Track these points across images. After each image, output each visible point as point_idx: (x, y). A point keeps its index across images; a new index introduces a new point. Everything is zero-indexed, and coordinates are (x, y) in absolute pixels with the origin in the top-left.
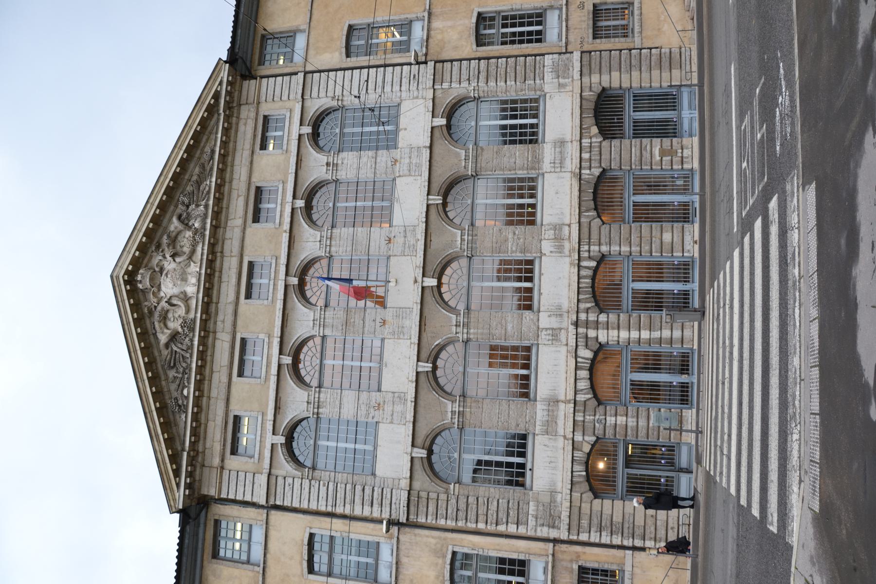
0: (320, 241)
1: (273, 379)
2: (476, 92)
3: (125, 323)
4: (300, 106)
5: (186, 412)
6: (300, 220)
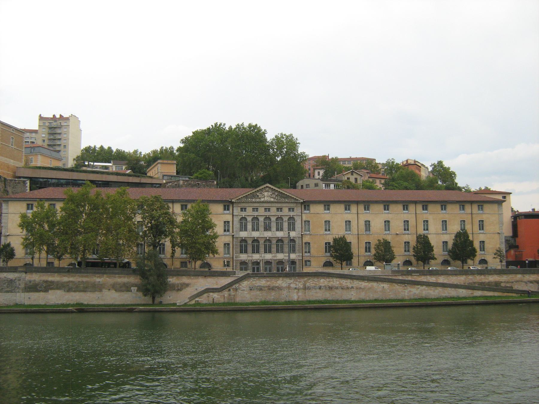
1: (252, 214)
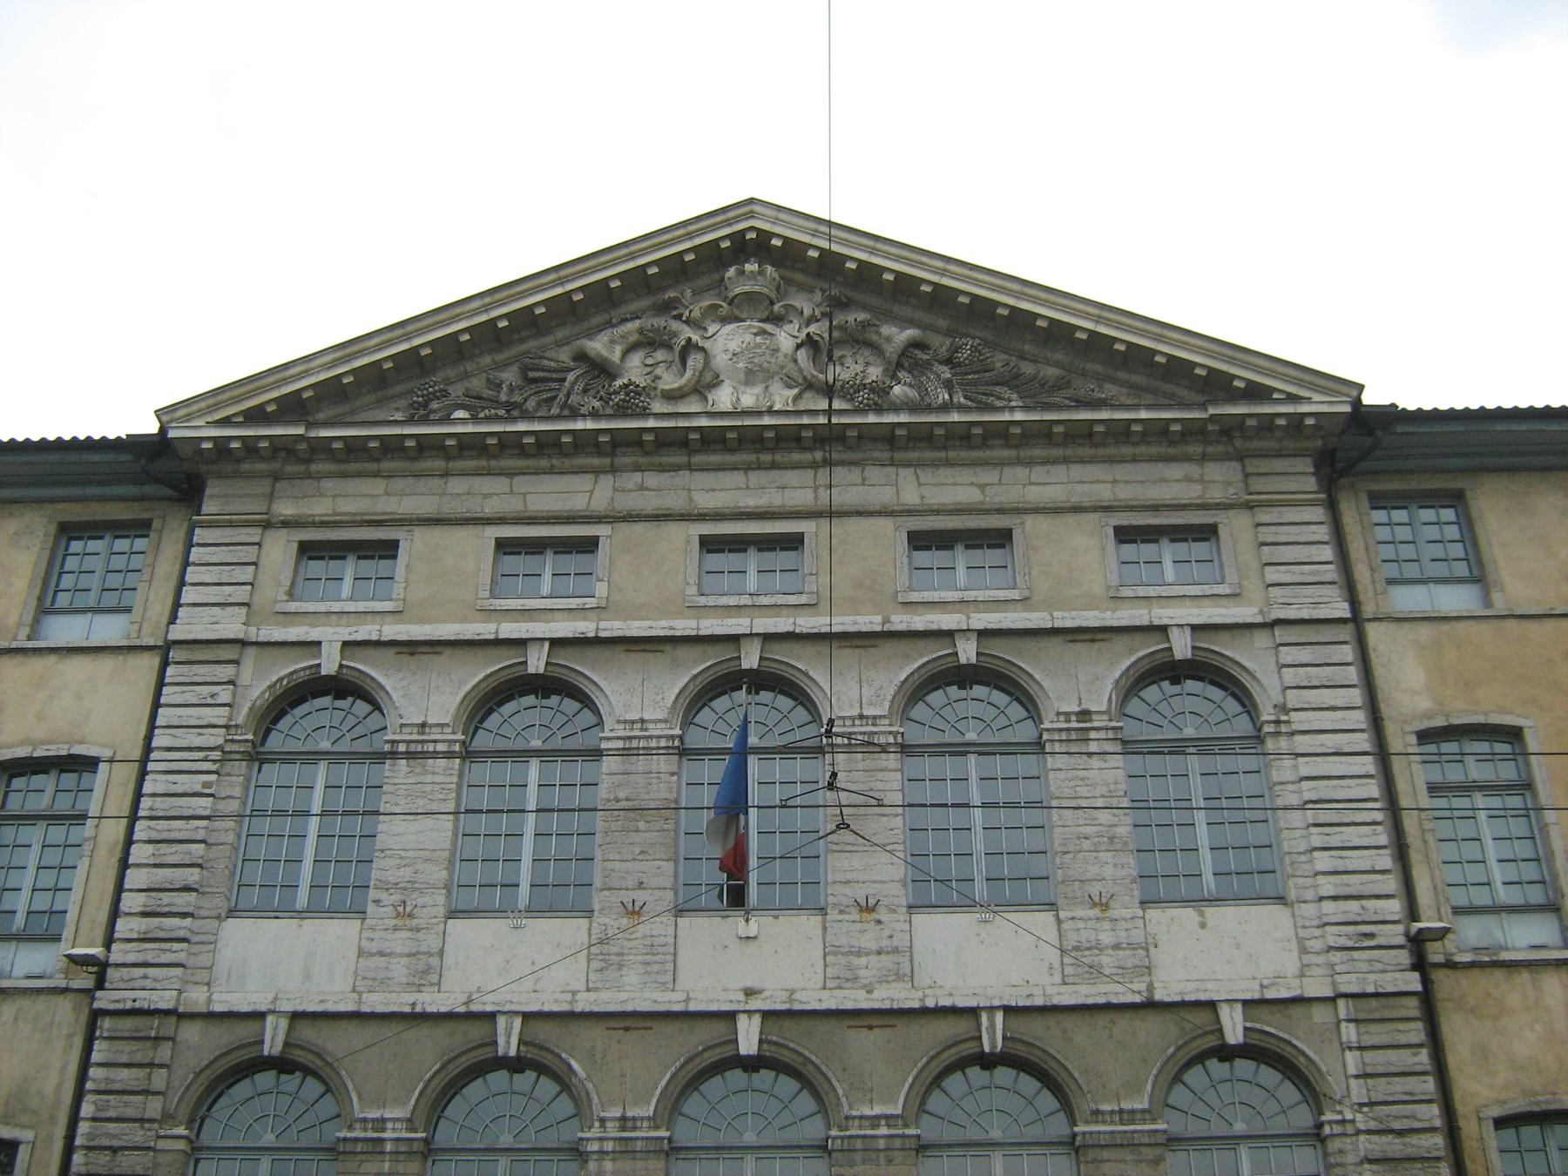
0: (861, 717)
1: (486, 630)
2: (1337, 1129)
3: (633, 248)
4: (1249, 620)
5: (410, 421)
6: (921, 655)
